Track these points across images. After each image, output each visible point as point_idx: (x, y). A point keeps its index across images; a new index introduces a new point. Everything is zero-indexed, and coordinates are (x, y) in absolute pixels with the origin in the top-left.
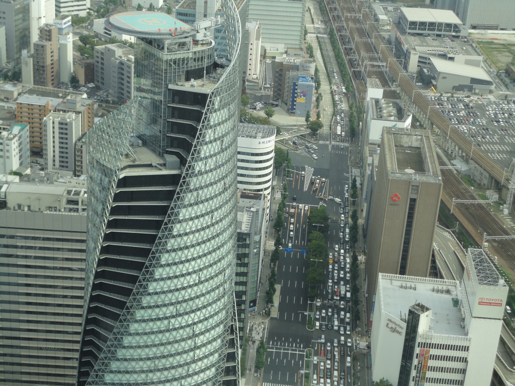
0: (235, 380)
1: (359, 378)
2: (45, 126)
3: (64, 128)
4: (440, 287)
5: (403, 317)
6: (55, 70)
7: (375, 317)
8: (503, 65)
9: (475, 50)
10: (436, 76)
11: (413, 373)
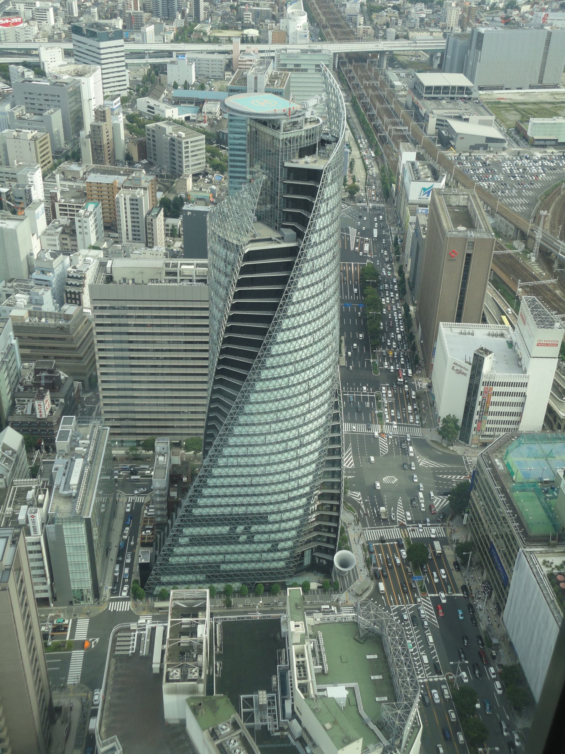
2: (118, 202)
3: (135, 203)
4: (495, 332)
5: (468, 360)
6: (111, 149)
7: (437, 361)
8: (513, 124)
9: (487, 110)
11: (478, 408)
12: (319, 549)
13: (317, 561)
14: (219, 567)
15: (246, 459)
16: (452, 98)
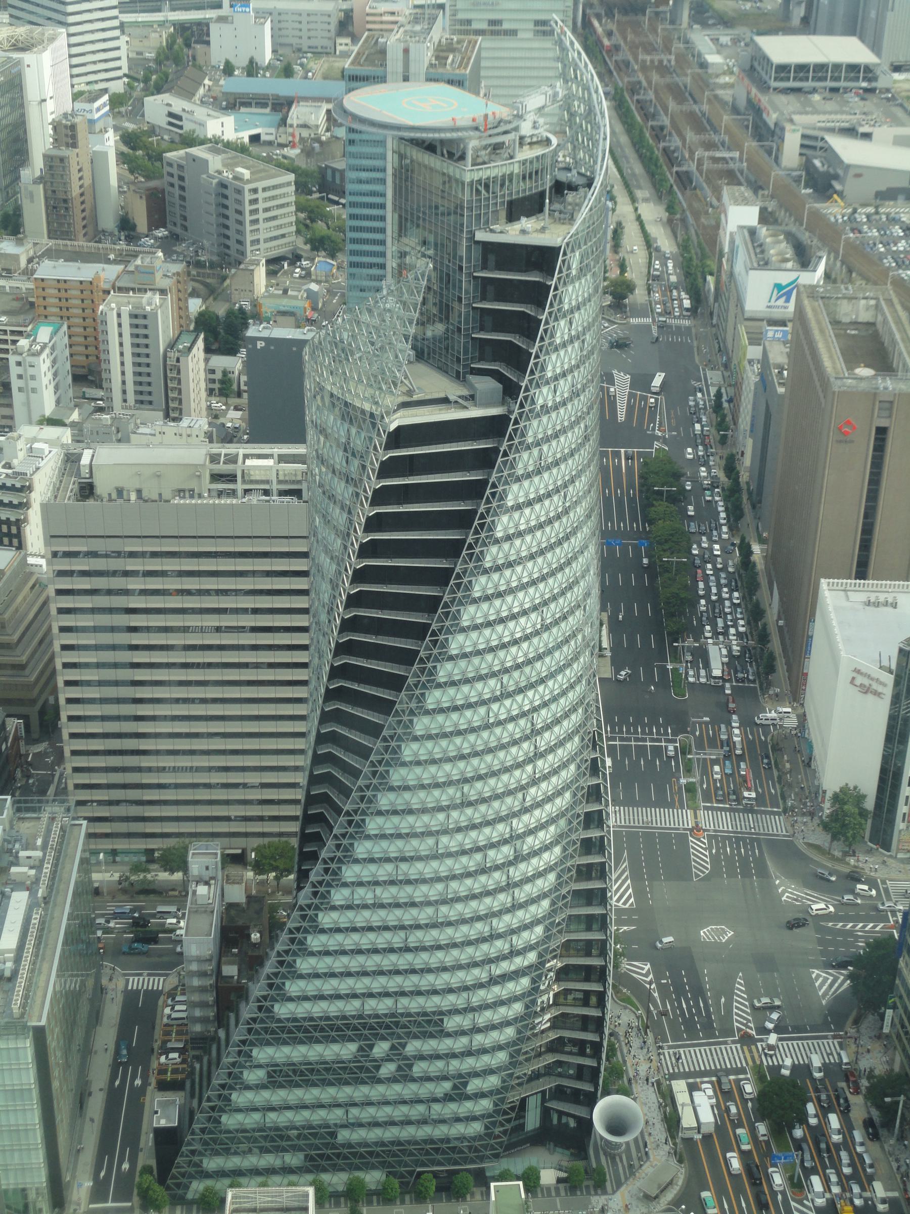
0: (600, 812)
1: (790, 786)
3: (141, 323)
5: (885, 663)
7: (816, 665)
10: (840, 172)
12: (559, 1093)
13: (555, 1121)
14: (333, 1135)
15: (393, 890)
16: (834, 90)
